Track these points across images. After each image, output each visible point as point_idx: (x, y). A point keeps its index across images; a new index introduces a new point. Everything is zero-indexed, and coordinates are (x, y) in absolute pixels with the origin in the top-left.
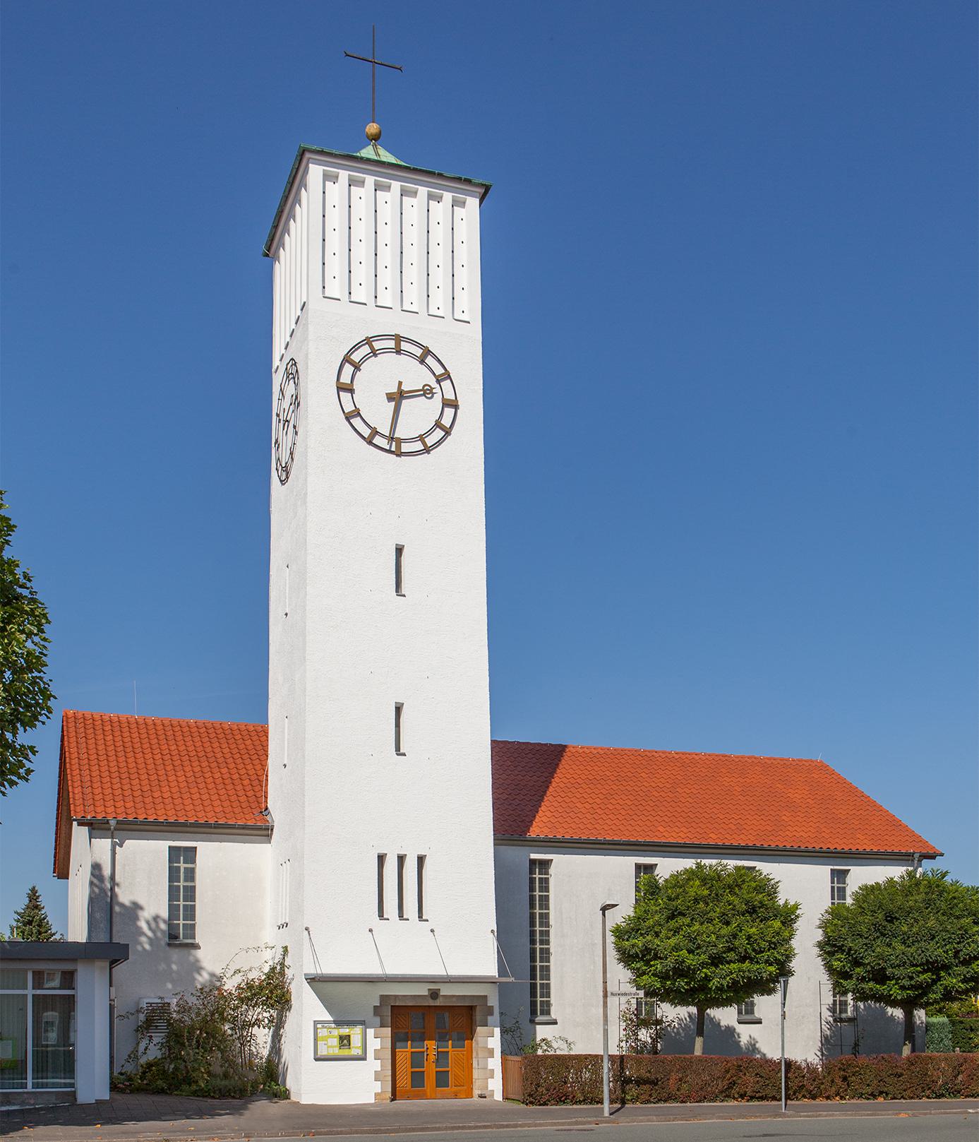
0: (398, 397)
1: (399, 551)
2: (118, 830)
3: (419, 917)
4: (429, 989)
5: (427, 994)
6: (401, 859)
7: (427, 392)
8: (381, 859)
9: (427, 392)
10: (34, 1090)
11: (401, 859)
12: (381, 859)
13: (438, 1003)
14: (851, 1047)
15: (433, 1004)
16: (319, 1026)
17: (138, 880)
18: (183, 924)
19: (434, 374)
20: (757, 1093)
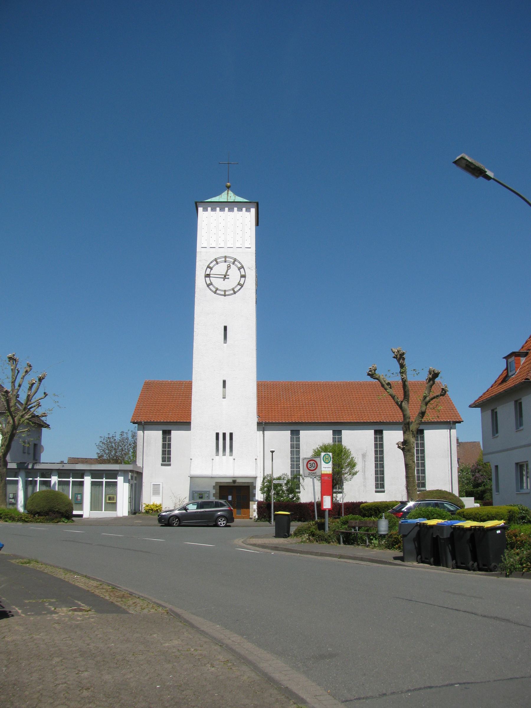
0: (225, 277)
1: (225, 328)
2: (145, 425)
3: (377, 487)
4: (233, 480)
5: (232, 481)
6: (224, 434)
7: (229, 267)
8: (217, 434)
9: (229, 267)
10: (105, 512)
11: (224, 434)
12: (217, 434)
13: (236, 484)
14: (346, 446)
15: (233, 485)
16: (194, 493)
17: (152, 442)
18: (167, 457)
19: (241, 274)
20: (237, 669)
